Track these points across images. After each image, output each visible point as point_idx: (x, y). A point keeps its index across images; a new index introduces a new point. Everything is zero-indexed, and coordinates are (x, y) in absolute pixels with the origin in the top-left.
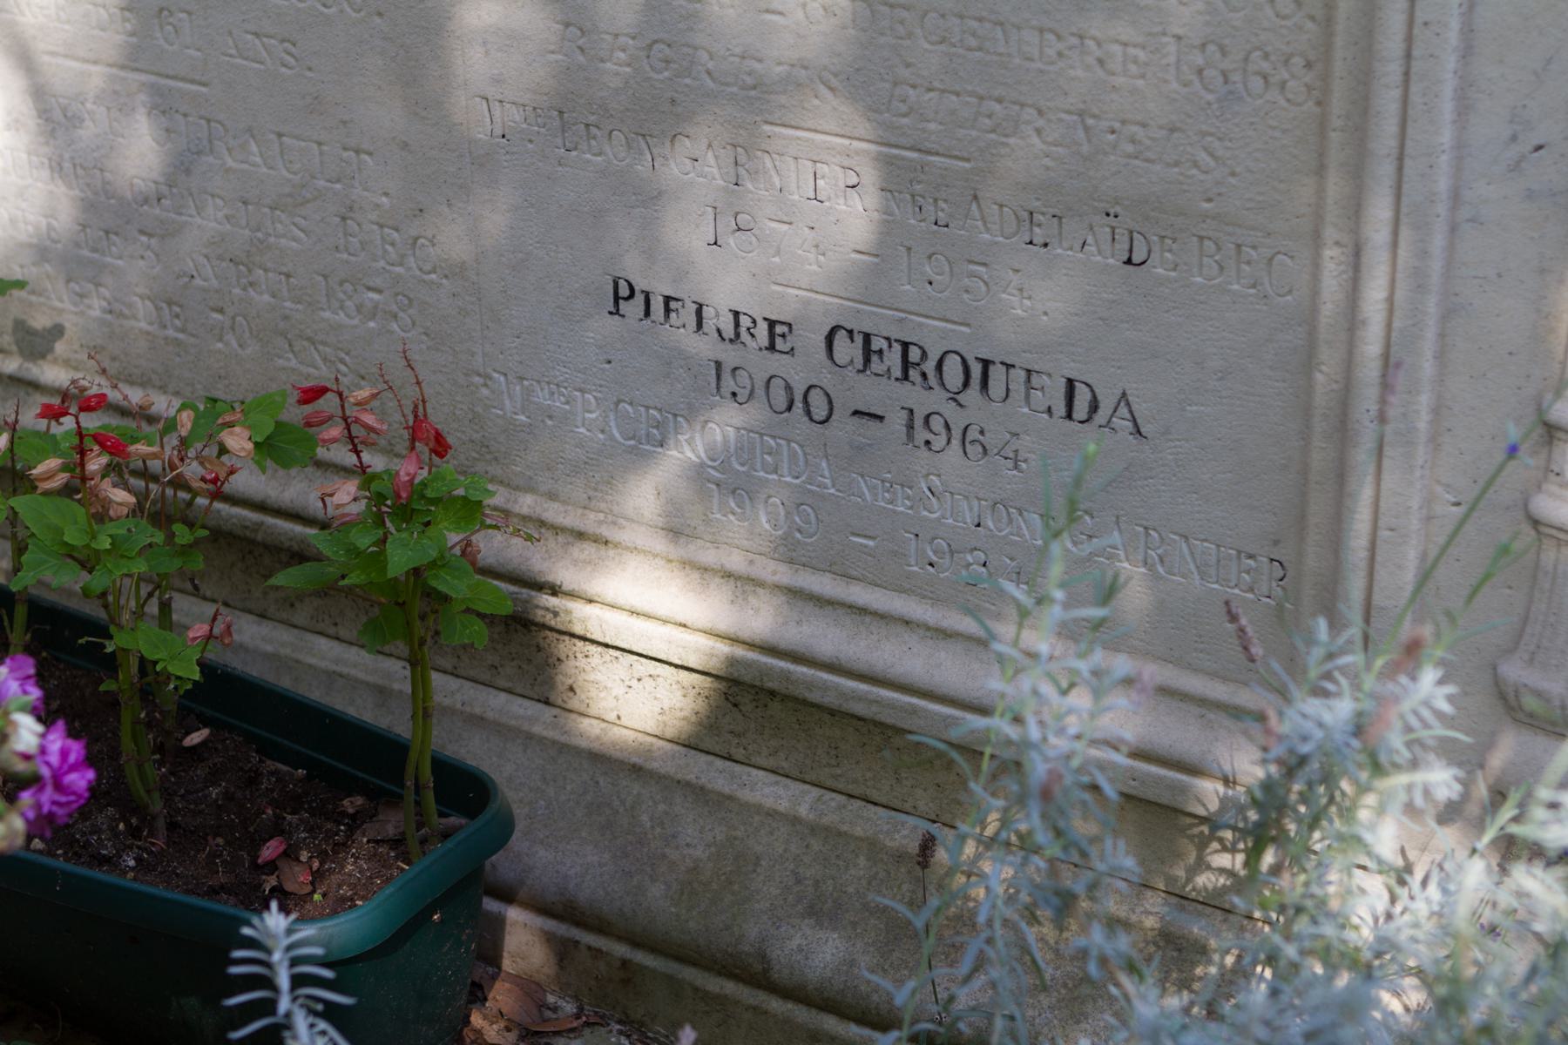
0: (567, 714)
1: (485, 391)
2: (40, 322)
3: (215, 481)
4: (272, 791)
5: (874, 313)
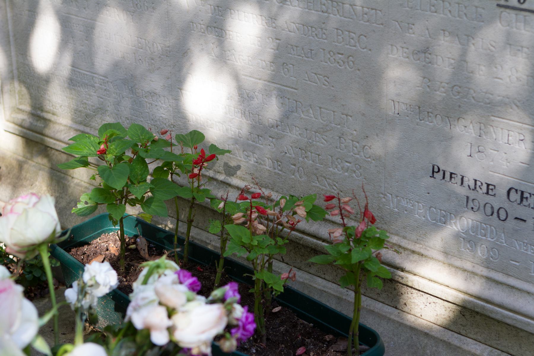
0: (403, 313)
1: (384, 200)
2: (233, 164)
3: (292, 224)
4: (301, 330)
5: (527, 185)
